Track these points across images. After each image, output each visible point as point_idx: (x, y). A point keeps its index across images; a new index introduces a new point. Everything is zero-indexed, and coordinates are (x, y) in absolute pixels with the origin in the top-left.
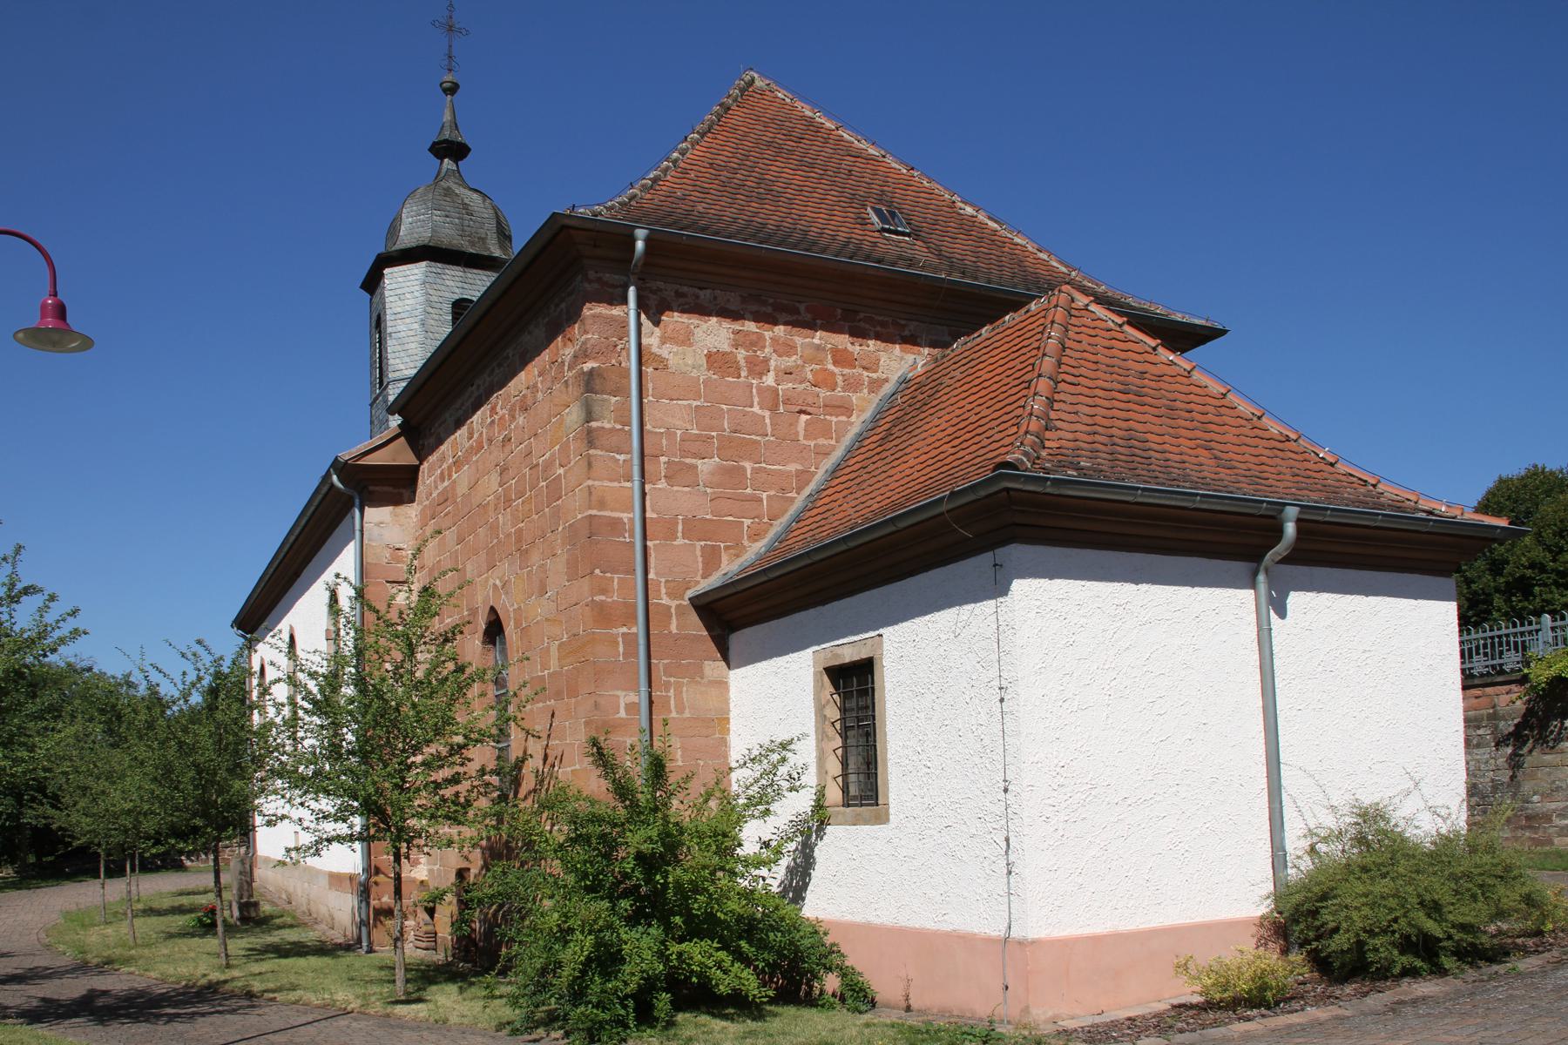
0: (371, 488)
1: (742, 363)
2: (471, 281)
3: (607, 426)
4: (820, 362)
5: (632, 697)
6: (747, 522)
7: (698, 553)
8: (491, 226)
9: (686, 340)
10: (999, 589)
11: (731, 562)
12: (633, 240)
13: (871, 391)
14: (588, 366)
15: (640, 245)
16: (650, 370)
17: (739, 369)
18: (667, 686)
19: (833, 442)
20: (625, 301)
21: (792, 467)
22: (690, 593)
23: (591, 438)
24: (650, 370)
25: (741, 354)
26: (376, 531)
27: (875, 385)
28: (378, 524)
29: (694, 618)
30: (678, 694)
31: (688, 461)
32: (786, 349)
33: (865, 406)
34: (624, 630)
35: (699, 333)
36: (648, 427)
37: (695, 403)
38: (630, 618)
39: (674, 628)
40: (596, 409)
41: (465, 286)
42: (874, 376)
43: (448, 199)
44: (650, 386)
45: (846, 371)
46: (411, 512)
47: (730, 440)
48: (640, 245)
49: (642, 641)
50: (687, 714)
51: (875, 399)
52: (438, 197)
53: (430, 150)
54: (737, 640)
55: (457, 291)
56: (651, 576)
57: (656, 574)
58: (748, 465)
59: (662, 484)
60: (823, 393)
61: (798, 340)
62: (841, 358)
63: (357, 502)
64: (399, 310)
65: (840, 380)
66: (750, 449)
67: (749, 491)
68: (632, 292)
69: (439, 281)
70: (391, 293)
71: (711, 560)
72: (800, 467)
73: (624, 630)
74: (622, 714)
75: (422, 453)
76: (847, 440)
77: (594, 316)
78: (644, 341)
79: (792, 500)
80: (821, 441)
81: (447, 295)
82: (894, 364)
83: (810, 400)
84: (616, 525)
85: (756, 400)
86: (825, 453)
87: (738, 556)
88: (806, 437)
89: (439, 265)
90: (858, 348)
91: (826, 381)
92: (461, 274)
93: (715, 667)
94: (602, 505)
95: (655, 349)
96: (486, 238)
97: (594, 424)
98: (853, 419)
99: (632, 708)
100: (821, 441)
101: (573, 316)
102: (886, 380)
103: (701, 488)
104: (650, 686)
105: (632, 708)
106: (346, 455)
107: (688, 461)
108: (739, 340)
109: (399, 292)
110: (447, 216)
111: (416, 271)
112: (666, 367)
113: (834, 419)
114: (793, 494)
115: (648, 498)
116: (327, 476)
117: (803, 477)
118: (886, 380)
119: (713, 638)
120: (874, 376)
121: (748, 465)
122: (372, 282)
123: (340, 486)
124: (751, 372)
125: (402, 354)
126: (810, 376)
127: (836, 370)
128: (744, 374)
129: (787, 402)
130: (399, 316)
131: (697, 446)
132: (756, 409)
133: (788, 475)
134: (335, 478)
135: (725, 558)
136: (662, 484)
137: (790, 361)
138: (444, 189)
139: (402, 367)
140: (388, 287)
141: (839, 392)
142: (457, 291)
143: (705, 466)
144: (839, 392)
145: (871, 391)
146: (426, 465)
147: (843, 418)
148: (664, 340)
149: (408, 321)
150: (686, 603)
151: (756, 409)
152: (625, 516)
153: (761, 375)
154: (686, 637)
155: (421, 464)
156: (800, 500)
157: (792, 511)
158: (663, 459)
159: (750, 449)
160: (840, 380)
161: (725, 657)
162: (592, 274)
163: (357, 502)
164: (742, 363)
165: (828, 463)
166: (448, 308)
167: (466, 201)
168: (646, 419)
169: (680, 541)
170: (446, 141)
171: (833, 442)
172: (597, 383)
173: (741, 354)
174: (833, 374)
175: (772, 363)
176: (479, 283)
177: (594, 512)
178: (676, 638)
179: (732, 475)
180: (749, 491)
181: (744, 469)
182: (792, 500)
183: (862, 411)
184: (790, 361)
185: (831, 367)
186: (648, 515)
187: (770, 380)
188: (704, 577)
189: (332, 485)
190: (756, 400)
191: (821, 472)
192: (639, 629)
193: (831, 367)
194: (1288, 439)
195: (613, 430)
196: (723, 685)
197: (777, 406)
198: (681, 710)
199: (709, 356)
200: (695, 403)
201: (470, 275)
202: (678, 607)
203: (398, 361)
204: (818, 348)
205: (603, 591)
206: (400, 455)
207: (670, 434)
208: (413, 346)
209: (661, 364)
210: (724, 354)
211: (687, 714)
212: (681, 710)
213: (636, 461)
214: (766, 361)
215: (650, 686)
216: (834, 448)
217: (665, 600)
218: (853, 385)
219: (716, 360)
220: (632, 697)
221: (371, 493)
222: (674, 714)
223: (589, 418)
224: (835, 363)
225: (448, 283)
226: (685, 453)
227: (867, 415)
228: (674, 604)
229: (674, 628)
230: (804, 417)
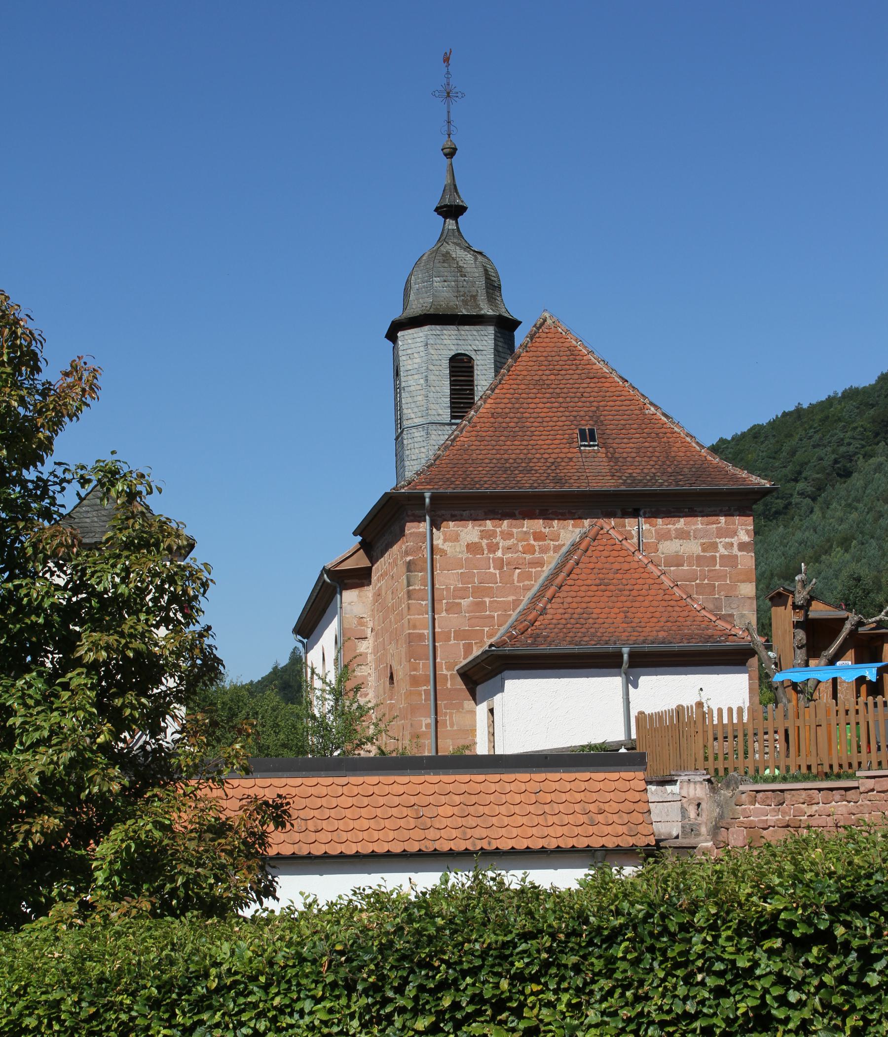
0: (346, 581)
1: (485, 547)
2: (464, 337)
3: (417, 588)
4: (527, 540)
5: (429, 721)
6: (486, 629)
7: (461, 647)
8: (481, 283)
9: (456, 538)
10: (501, 689)
11: (478, 650)
12: (424, 498)
13: (555, 552)
14: (408, 559)
15: (427, 500)
16: (438, 557)
17: (483, 550)
18: (446, 714)
19: (533, 582)
20: (425, 521)
21: (510, 598)
22: (457, 668)
23: (410, 594)
24: (438, 557)
25: (484, 542)
26: (349, 607)
27: (557, 549)
28: (350, 604)
29: (459, 679)
30: (451, 717)
31: (456, 601)
32: (507, 536)
33: (552, 559)
34: (425, 688)
35: (463, 535)
36: (437, 586)
37: (460, 571)
38: (427, 683)
39: (449, 686)
40: (412, 580)
41: (460, 342)
42: (557, 543)
43: (446, 265)
44: (438, 565)
45: (541, 543)
46: (368, 592)
47: (478, 587)
48: (427, 500)
49: (432, 693)
50: (455, 728)
51: (557, 556)
52: (438, 265)
53: (436, 210)
54: (479, 689)
55: (453, 347)
56: (438, 660)
57: (441, 659)
58: (487, 600)
59: (444, 614)
60: (528, 557)
61: (515, 530)
62: (538, 537)
63: (338, 589)
64: (410, 367)
65: (537, 548)
66: (489, 592)
67: (488, 613)
68: (428, 518)
69: (438, 341)
70: (404, 353)
71: (468, 649)
72: (514, 598)
73: (425, 688)
74: (424, 729)
75: (373, 560)
76: (541, 580)
77: (411, 534)
78: (435, 543)
79: (510, 615)
80: (526, 583)
81: (445, 352)
82: (569, 535)
83: (520, 562)
84: (421, 637)
85: (492, 565)
86: (527, 589)
87: (481, 647)
88: (518, 582)
89: (438, 327)
90: (548, 529)
91: (530, 550)
92: (456, 332)
93: (469, 704)
94: (415, 627)
95: (440, 546)
96: (477, 295)
97: (411, 588)
98: (545, 568)
99: (428, 726)
100: (526, 583)
101: (402, 533)
102: (564, 545)
103: (463, 614)
104: (436, 714)
105: (428, 726)
106: (329, 564)
107: (456, 601)
108: (484, 535)
109: (409, 352)
110: (445, 281)
111: (421, 334)
112: (446, 554)
113: (534, 570)
114: (511, 612)
115: (436, 622)
116: (321, 575)
117: (516, 603)
118: (564, 545)
119: (469, 689)
120: (557, 543)
121: (487, 600)
122: (392, 336)
123: (328, 580)
124: (490, 551)
125: (413, 406)
126: (521, 549)
127: (535, 543)
128: (486, 552)
129: (508, 564)
130: (409, 373)
131: (461, 593)
132: (492, 570)
133: (509, 602)
134: (325, 576)
135: (475, 648)
136: (444, 614)
137: (509, 543)
138: (443, 255)
139: (413, 416)
140: (401, 348)
141: (537, 555)
142: (453, 347)
143: (465, 602)
144: (537, 555)
145: (555, 552)
146: (376, 566)
147: (539, 569)
148: (445, 541)
149: (416, 377)
150: (455, 672)
151: (492, 570)
152: (426, 632)
153: (494, 552)
154: (455, 690)
155: (373, 565)
156: (514, 615)
157: (510, 621)
158: (444, 601)
159: (489, 592)
160: (537, 548)
161: (474, 699)
162: (410, 513)
163: (338, 589)
164: (485, 547)
165: (530, 594)
166: (446, 363)
167: (461, 264)
168: (436, 582)
169: (452, 642)
170: (446, 206)
171: (533, 582)
172: (412, 568)
173: (484, 542)
174: (534, 546)
175: (501, 544)
176: (470, 337)
177: (411, 631)
178: (450, 690)
179: (479, 606)
180: (488, 613)
181: (485, 602)
182: (510, 615)
183: (550, 563)
184: (509, 543)
185: (532, 542)
186: (436, 630)
187: (499, 554)
188: (464, 659)
189: (324, 581)
190: (492, 565)
191: (526, 599)
192: (431, 687)
193: (532, 542)
194: (682, 599)
195: (420, 589)
196: (474, 713)
197: (502, 567)
198: (452, 725)
199: (468, 546)
200: (460, 571)
201: (463, 333)
202: (451, 675)
203: (410, 411)
204: (525, 533)
205: (415, 670)
206: (361, 561)
207: (448, 589)
208: (420, 398)
209: (443, 553)
210: (476, 543)
211: (455, 728)
212: (452, 725)
213: (430, 605)
214: (498, 544)
215: (436, 714)
216: (533, 585)
217: (445, 672)
218: (544, 550)
219: (472, 548)
220: (429, 721)
221: (346, 584)
222: (449, 728)
223: (409, 585)
224: (535, 540)
225: (445, 342)
226: (455, 597)
227: (552, 565)
228: (449, 673)
229: (449, 686)
230: (518, 571)
